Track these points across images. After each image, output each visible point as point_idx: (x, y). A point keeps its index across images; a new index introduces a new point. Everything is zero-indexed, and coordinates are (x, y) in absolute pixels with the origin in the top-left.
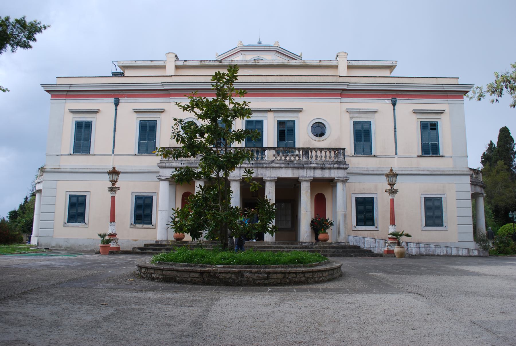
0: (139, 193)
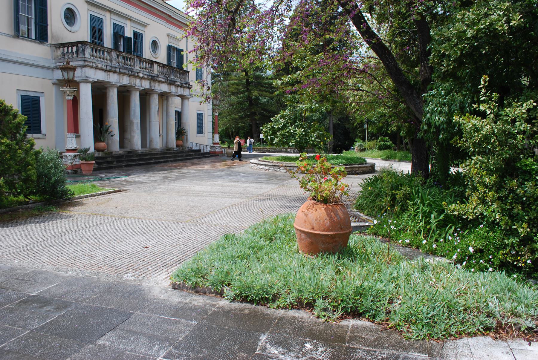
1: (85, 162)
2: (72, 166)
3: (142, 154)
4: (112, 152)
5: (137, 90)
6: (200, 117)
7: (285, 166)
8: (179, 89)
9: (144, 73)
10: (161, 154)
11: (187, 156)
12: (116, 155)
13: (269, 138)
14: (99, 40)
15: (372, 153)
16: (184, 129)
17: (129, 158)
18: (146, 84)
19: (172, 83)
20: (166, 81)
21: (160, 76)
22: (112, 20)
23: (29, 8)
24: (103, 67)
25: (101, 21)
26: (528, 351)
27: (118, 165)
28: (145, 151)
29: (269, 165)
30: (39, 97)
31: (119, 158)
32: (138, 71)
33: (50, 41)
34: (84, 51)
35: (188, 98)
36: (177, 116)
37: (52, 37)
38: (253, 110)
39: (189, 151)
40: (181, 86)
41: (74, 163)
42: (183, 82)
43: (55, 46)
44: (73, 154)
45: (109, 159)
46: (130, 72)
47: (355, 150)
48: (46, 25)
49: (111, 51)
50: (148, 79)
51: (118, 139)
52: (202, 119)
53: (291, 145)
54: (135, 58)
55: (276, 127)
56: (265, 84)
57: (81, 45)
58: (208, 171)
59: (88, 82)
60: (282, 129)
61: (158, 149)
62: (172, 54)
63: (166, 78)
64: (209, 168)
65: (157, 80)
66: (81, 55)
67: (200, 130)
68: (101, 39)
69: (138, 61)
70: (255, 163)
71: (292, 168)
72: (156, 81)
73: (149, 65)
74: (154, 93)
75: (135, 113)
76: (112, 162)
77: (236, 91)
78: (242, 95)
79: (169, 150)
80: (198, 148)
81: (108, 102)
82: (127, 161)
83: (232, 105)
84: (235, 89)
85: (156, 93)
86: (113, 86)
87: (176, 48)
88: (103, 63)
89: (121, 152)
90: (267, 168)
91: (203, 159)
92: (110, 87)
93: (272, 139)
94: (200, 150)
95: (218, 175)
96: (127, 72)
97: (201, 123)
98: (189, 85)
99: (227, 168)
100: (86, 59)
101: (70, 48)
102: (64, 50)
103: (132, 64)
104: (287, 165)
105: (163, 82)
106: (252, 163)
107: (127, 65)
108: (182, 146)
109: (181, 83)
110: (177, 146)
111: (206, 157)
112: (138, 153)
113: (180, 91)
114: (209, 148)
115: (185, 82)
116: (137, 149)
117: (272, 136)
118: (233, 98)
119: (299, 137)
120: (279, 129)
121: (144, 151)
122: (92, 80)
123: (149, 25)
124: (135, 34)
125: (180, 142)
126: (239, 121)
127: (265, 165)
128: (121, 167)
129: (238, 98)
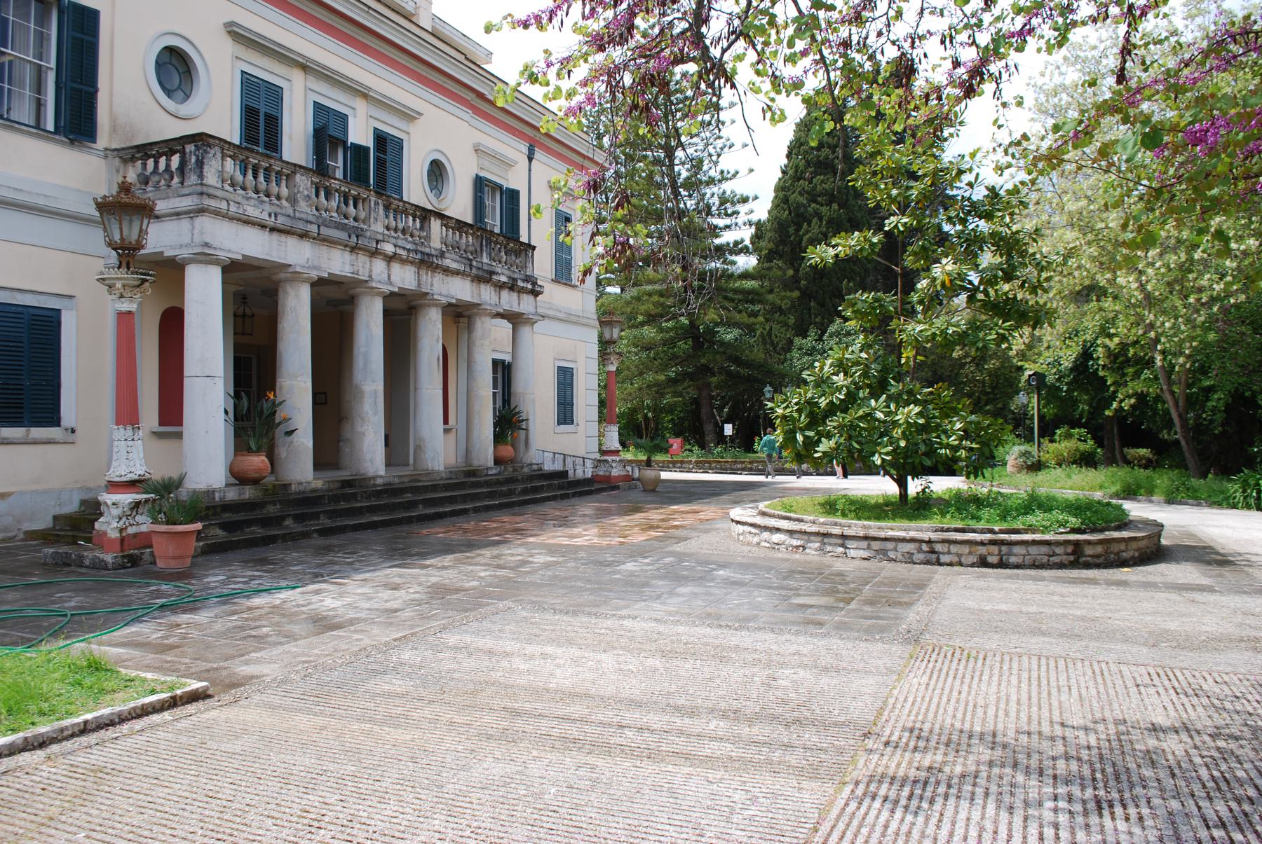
0: (8, 293)
1: (164, 528)
2: (122, 540)
3: (390, 490)
4: (286, 486)
5: (374, 292)
6: (565, 378)
7: (866, 538)
8: (505, 294)
9: (400, 243)
10: (448, 487)
11: (525, 491)
12: (300, 493)
13: (800, 438)
14: (266, 147)
15: (1069, 476)
16: (520, 412)
17: (343, 505)
18: (404, 278)
19: (484, 277)
20: (468, 269)
21: (447, 255)
22: (309, 92)
23: (41, 39)
24: (265, 216)
25: (275, 94)
26: (271, 222)
27: (298, 528)
28: (396, 480)
29: (805, 532)
30: (59, 311)
31: (307, 503)
32: (380, 237)
33: (104, 139)
34: (200, 164)
35: (532, 323)
36: (499, 376)
37: (114, 129)
38: (703, 361)
39: (531, 478)
40: (512, 287)
41: (131, 530)
42: (516, 276)
43: (121, 154)
44: (127, 498)
45: (272, 510)
46: (354, 239)
47: (1009, 468)
48: (91, 90)
49: (294, 173)
50: (412, 263)
51: (310, 444)
52: (572, 384)
53: (879, 462)
54: (373, 199)
55: (823, 402)
56: (736, 291)
57: (193, 148)
58: (598, 560)
59: (211, 263)
60: (844, 407)
61: (439, 472)
62: (488, 203)
63: (467, 262)
64: (596, 540)
65: (437, 266)
66: (192, 179)
67: (565, 414)
68: (273, 143)
69: (381, 207)
70: (752, 525)
71: (890, 545)
72: (434, 268)
73: (414, 220)
74: (429, 306)
75: (366, 362)
76: (277, 521)
77: (659, 310)
78: (671, 324)
79: (472, 473)
80: (558, 467)
81: (280, 327)
82: (333, 514)
83: (648, 348)
84: (656, 304)
85: (435, 304)
86: (297, 277)
87: (501, 187)
88: (267, 208)
89: (319, 484)
90: (799, 543)
91: (574, 501)
92: (286, 280)
93: (811, 444)
94: (564, 474)
95: (632, 574)
96: (342, 235)
97: (568, 393)
98: (534, 284)
99: (657, 538)
100: (205, 189)
101: (163, 160)
102: (145, 165)
103: (362, 215)
104: (872, 533)
105: (457, 273)
106: (738, 522)
107: (346, 217)
108: (512, 461)
109: (509, 277)
110: (497, 461)
111: (581, 494)
112: (375, 485)
113: (509, 301)
114: (589, 464)
115: (522, 277)
116: (371, 473)
117: (808, 433)
118: (649, 332)
119: (903, 433)
120: (832, 410)
121: (398, 475)
122: (223, 255)
123: (421, 114)
124: (382, 140)
125: (507, 451)
126: (666, 390)
127: (791, 533)
128: (306, 535)
129: (661, 330)
